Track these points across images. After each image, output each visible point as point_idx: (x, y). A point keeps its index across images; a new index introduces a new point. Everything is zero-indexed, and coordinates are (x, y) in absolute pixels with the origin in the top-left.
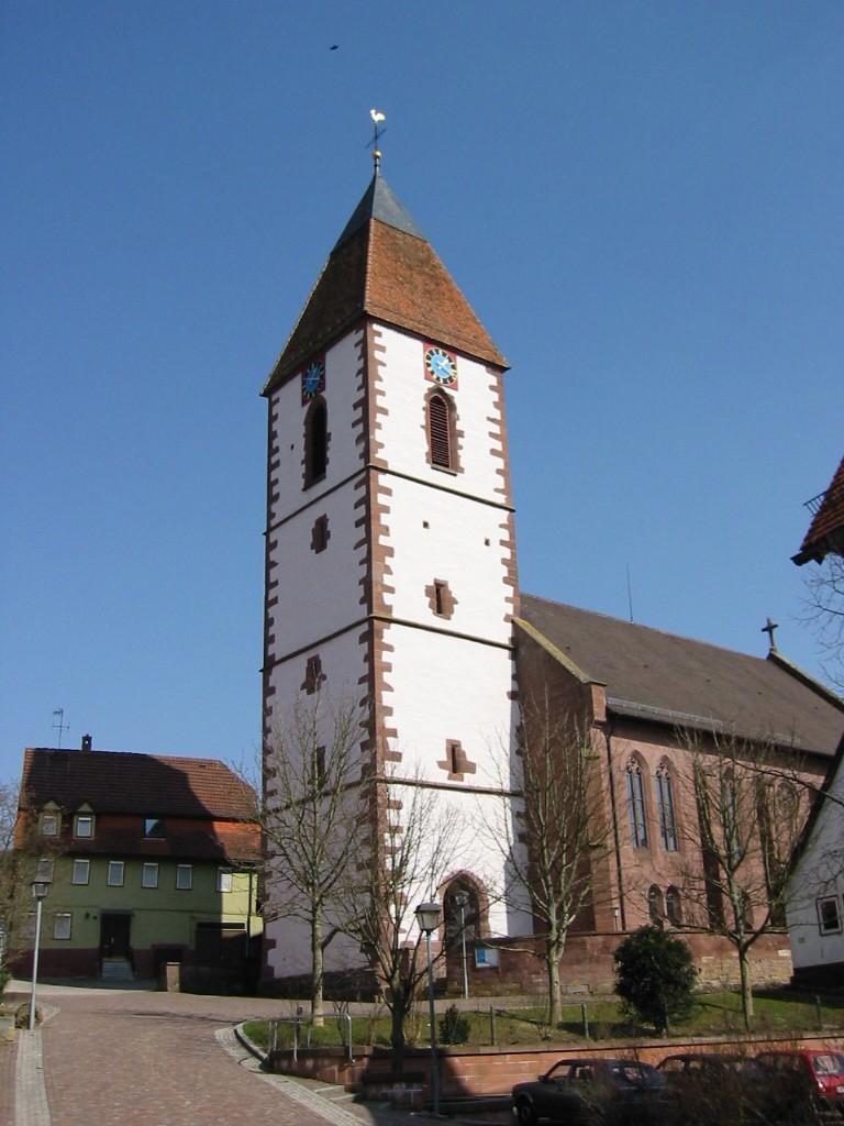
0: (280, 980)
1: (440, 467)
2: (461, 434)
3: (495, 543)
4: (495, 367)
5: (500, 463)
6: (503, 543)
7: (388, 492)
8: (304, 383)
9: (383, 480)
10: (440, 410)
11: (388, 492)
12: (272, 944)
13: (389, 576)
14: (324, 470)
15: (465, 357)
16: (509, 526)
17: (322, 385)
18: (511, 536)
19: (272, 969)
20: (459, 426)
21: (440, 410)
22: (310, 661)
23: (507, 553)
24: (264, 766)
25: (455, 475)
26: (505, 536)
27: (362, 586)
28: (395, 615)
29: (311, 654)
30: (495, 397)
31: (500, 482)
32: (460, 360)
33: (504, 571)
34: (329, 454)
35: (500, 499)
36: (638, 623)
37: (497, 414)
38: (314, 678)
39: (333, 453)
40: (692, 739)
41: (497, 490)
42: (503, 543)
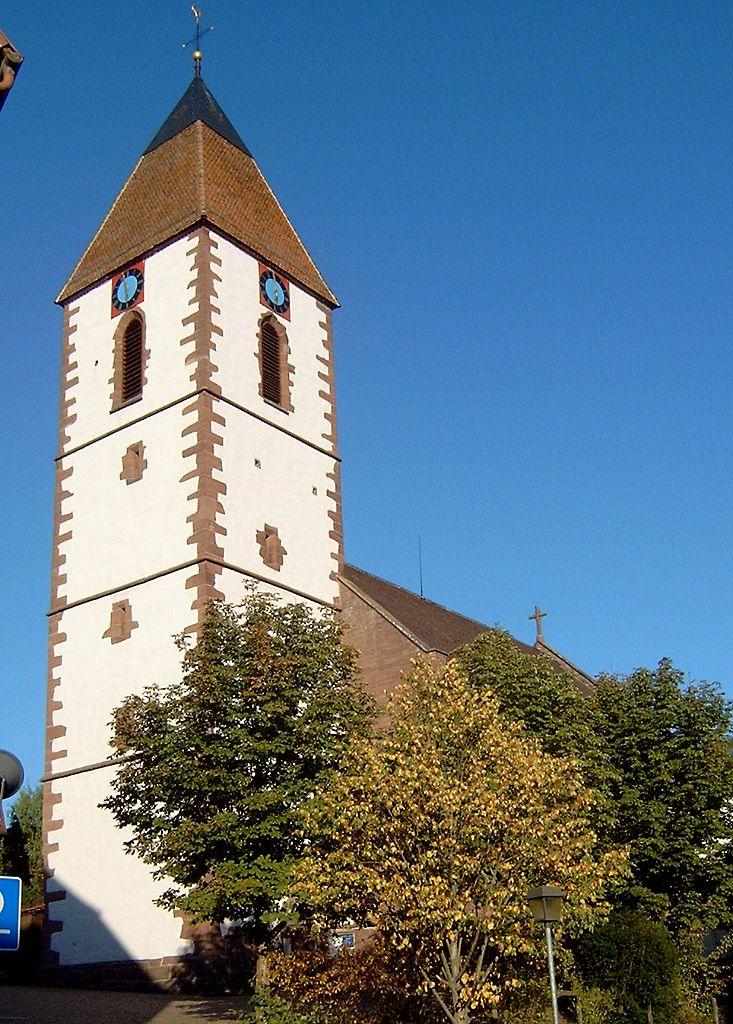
0: (67, 968)
1: (271, 402)
2: (291, 369)
3: (321, 492)
4: (323, 301)
5: (327, 407)
6: (329, 493)
7: (222, 421)
8: (115, 292)
9: (218, 407)
10: (271, 343)
11: (222, 421)
12: (58, 926)
13: (223, 496)
14: (140, 391)
15: (297, 286)
16: (336, 476)
17: (138, 296)
18: (339, 507)
19: (56, 955)
20: (291, 360)
21: (271, 343)
22: (115, 606)
23: (332, 505)
24: (141, 278)
25: (288, 414)
26: (331, 486)
27: (191, 524)
28: (227, 560)
29: (119, 597)
30: (324, 335)
31: (327, 427)
32: (293, 289)
33: (330, 525)
34: (147, 373)
35: (328, 446)
36: (427, 598)
37: (325, 355)
38: (121, 626)
39: (151, 371)
40: (486, 962)
41: (324, 435)
42: (329, 493)
